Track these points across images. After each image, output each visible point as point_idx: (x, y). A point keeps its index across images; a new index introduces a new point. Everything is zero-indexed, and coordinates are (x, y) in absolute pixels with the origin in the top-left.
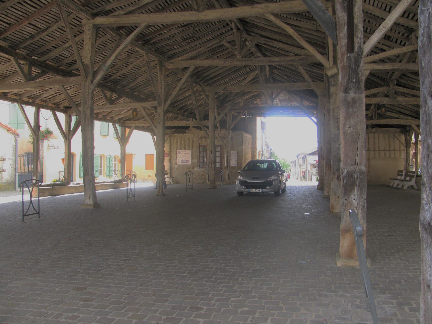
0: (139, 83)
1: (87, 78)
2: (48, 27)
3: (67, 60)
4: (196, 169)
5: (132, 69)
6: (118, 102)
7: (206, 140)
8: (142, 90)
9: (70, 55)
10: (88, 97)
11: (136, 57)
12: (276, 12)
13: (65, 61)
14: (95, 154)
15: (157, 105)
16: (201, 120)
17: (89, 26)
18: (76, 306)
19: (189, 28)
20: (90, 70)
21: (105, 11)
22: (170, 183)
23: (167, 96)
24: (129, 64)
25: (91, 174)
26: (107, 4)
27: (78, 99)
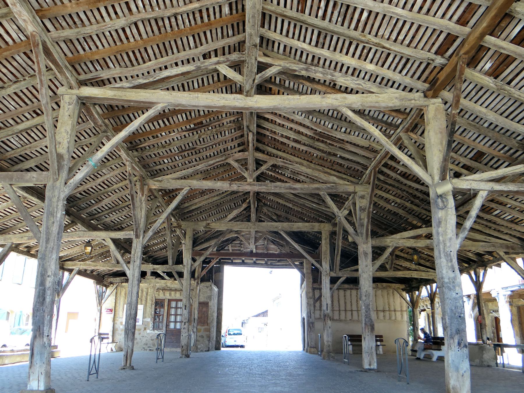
0: (102, 207)
1: (59, 175)
3: (13, 152)
4: (148, 331)
5: (100, 185)
6: (74, 227)
7: (164, 293)
8: (103, 217)
9: (19, 146)
10: (57, 205)
11: (111, 168)
13: (8, 154)
14: (271, 272)
15: (133, 237)
16: (173, 265)
17: (71, 98)
19: (193, 134)
20: (65, 163)
21: (100, 79)
22: (112, 350)
23: (149, 224)
24: (99, 176)
25: (47, 335)
26: (102, 69)
27: (9, 222)
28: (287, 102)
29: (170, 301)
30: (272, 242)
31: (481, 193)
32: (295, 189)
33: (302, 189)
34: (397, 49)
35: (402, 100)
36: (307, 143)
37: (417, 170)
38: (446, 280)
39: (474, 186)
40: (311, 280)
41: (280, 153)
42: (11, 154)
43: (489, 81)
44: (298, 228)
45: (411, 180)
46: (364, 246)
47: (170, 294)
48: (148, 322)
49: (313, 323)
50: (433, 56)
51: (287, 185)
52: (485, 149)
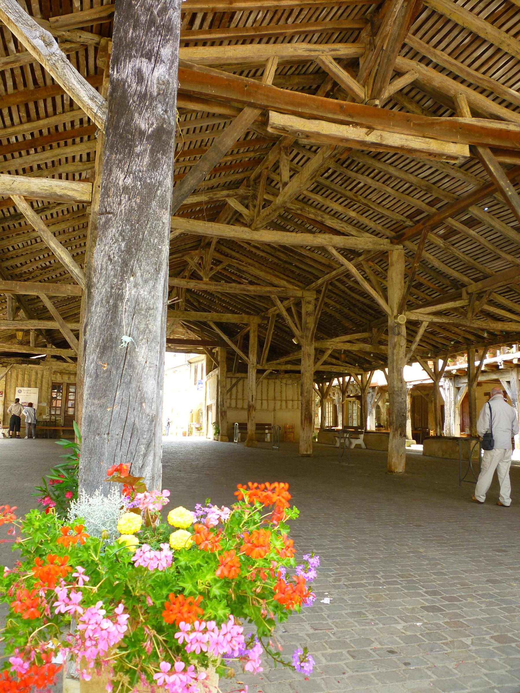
2: (45, 208)
12: (338, 246)
18: (296, 679)
28: (286, 238)
29: (68, 385)
30: (182, 326)
31: (424, 323)
32: (248, 291)
33: (255, 291)
34: (379, 210)
35: (374, 244)
36: (269, 251)
37: (381, 302)
38: (396, 389)
39: (421, 318)
40: (225, 369)
41: (234, 254)
42: (9, 254)
43: (440, 242)
44: (228, 319)
45: (356, 293)
46: (308, 348)
47: (69, 378)
48: (44, 407)
49: (225, 412)
50: (405, 219)
51: (242, 286)
52: (425, 282)
